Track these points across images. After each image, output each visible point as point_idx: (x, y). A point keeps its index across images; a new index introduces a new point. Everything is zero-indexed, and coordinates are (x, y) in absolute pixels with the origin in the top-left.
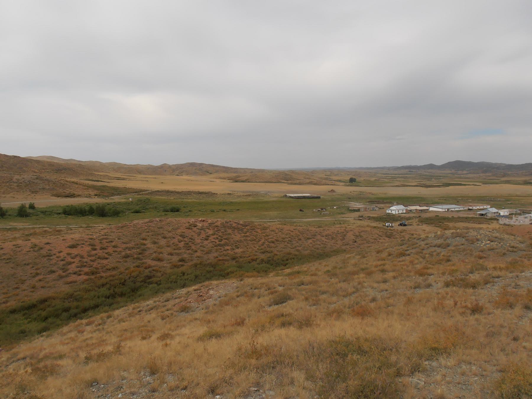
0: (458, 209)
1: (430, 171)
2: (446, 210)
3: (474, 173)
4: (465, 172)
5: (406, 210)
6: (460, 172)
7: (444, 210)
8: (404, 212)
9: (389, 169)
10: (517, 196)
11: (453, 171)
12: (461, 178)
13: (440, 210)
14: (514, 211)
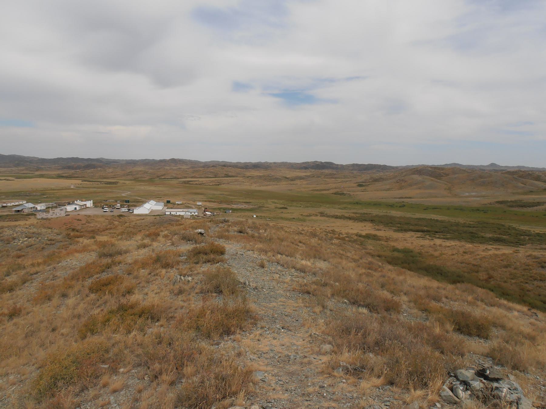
3: (4, 167)
14: (50, 204)
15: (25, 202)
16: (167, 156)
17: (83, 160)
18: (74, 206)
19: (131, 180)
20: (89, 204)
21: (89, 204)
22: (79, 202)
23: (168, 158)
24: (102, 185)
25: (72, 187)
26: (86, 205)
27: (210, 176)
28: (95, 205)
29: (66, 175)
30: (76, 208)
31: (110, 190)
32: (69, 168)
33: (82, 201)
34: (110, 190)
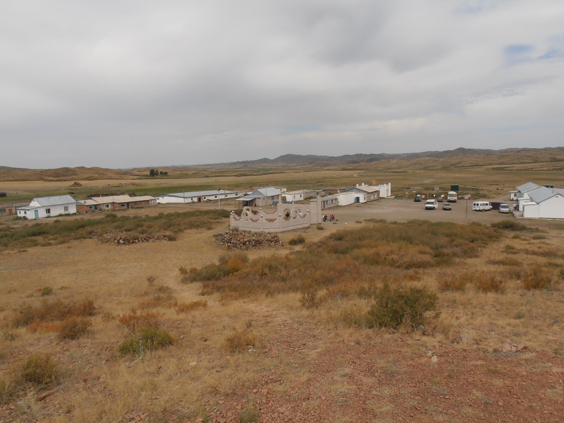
0: (223, 197)
1: (264, 164)
2: (195, 200)
4: (295, 164)
5: (79, 207)
6: (290, 165)
7: (189, 200)
8: (73, 210)
9: (225, 164)
10: (332, 178)
11: (284, 164)
12: (289, 169)
13: (181, 200)
15: (285, 190)
16: (452, 147)
17: (366, 155)
18: (354, 195)
19: (420, 169)
20: (385, 190)
21: (385, 190)
22: (364, 187)
23: (452, 148)
24: (389, 174)
25: (355, 176)
26: (378, 192)
27: (527, 161)
28: (397, 194)
29: (350, 168)
30: (358, 199)
31: (402, 177)
32: (354, 162)
33: (370, 184)
34: (402, 177)
